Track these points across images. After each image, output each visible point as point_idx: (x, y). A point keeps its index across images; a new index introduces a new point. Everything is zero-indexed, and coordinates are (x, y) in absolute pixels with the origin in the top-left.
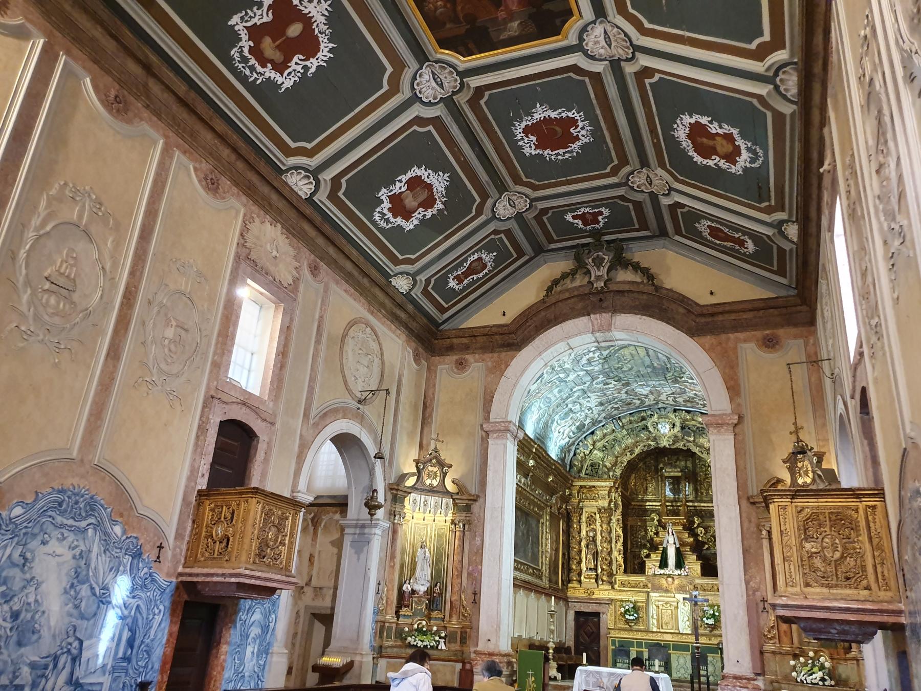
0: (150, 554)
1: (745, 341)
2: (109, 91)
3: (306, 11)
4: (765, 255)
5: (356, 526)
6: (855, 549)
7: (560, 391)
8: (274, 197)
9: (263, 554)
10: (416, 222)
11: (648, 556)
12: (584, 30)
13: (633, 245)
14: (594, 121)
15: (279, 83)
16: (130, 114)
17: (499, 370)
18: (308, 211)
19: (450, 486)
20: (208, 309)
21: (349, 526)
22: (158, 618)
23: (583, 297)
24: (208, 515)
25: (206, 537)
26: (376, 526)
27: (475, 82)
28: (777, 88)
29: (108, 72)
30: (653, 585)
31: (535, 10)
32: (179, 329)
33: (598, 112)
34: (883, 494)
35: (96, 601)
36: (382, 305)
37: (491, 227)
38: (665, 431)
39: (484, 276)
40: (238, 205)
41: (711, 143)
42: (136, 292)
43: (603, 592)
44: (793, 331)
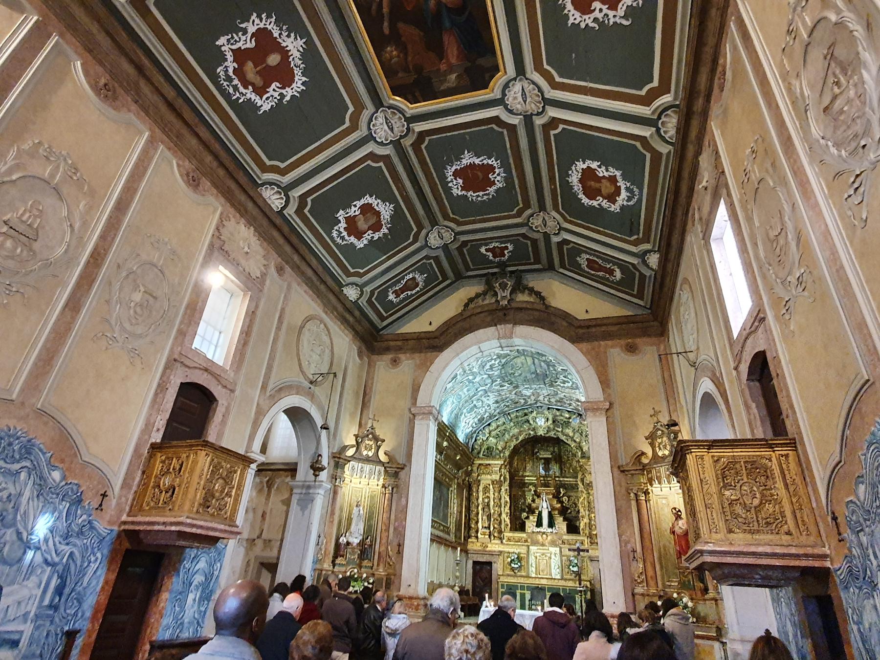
0: (91, 501)
1: (612, 347)
2: (100, 78)
3: (284, 44)
4: (630, 281)
5: (303, 487)
6: (772, 495)
7: (468, 390)
8: (250, 205)
9: (208, 504)
10: (366, 242)
11: (527, 518)
12: (506, 86)
13: (529, 276)
14: (508, 170)
15: (258, 105)
16: (118, 103)
17: (425, 367)
18: (278, 221)
19: (383, 457)
20: (179, 284)
21: (298, 487)
22: (94, 566)
23: (491, 312)
24: (158, 466)
25: (154, 488)
26: (320, 487)
27: (419, 127)
28: (658, 130)
29: (101, 63)
30: (532, 540)
31: (470, 64)
32: (147, 296)
33: (511, 161)
34: (795, 443)
35: (23, 546)
36: (335, 308)
37: (424, 253)
38: (541, 424)
39: (416, 293)
40: (217, 204)
41: (597, 185)
42: (105, 255)
43: (494, 546)
44: (645, 339)
